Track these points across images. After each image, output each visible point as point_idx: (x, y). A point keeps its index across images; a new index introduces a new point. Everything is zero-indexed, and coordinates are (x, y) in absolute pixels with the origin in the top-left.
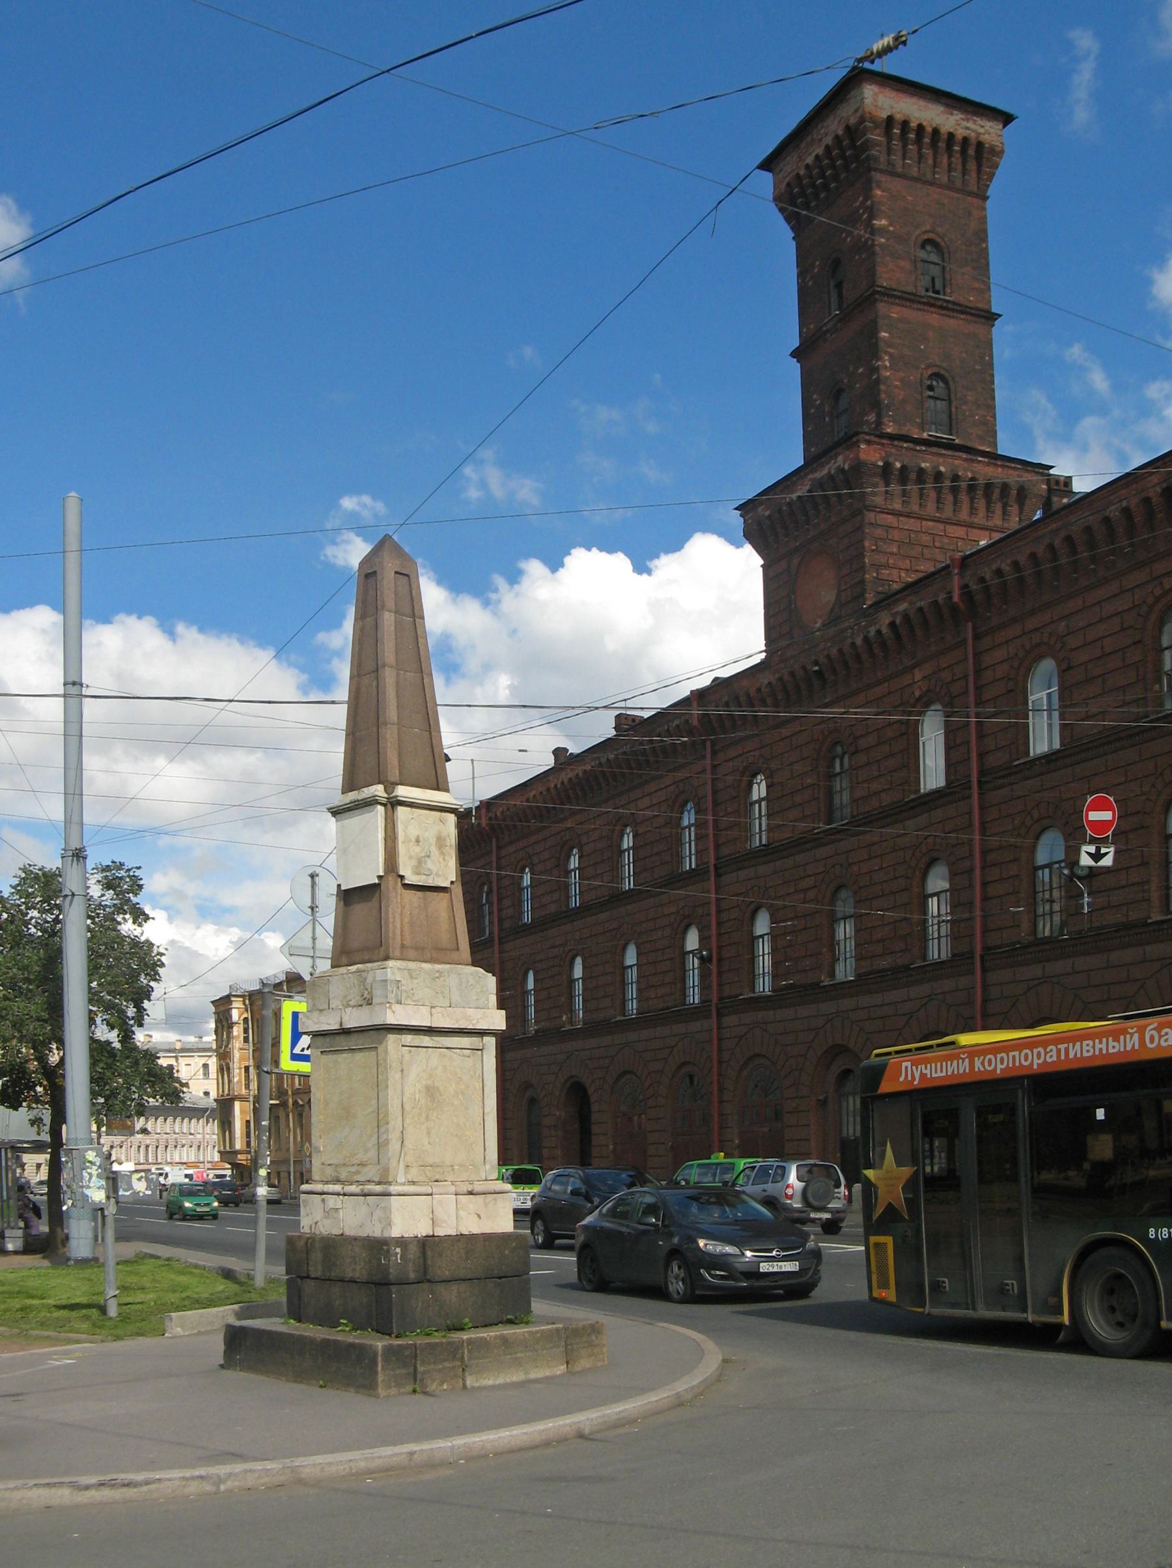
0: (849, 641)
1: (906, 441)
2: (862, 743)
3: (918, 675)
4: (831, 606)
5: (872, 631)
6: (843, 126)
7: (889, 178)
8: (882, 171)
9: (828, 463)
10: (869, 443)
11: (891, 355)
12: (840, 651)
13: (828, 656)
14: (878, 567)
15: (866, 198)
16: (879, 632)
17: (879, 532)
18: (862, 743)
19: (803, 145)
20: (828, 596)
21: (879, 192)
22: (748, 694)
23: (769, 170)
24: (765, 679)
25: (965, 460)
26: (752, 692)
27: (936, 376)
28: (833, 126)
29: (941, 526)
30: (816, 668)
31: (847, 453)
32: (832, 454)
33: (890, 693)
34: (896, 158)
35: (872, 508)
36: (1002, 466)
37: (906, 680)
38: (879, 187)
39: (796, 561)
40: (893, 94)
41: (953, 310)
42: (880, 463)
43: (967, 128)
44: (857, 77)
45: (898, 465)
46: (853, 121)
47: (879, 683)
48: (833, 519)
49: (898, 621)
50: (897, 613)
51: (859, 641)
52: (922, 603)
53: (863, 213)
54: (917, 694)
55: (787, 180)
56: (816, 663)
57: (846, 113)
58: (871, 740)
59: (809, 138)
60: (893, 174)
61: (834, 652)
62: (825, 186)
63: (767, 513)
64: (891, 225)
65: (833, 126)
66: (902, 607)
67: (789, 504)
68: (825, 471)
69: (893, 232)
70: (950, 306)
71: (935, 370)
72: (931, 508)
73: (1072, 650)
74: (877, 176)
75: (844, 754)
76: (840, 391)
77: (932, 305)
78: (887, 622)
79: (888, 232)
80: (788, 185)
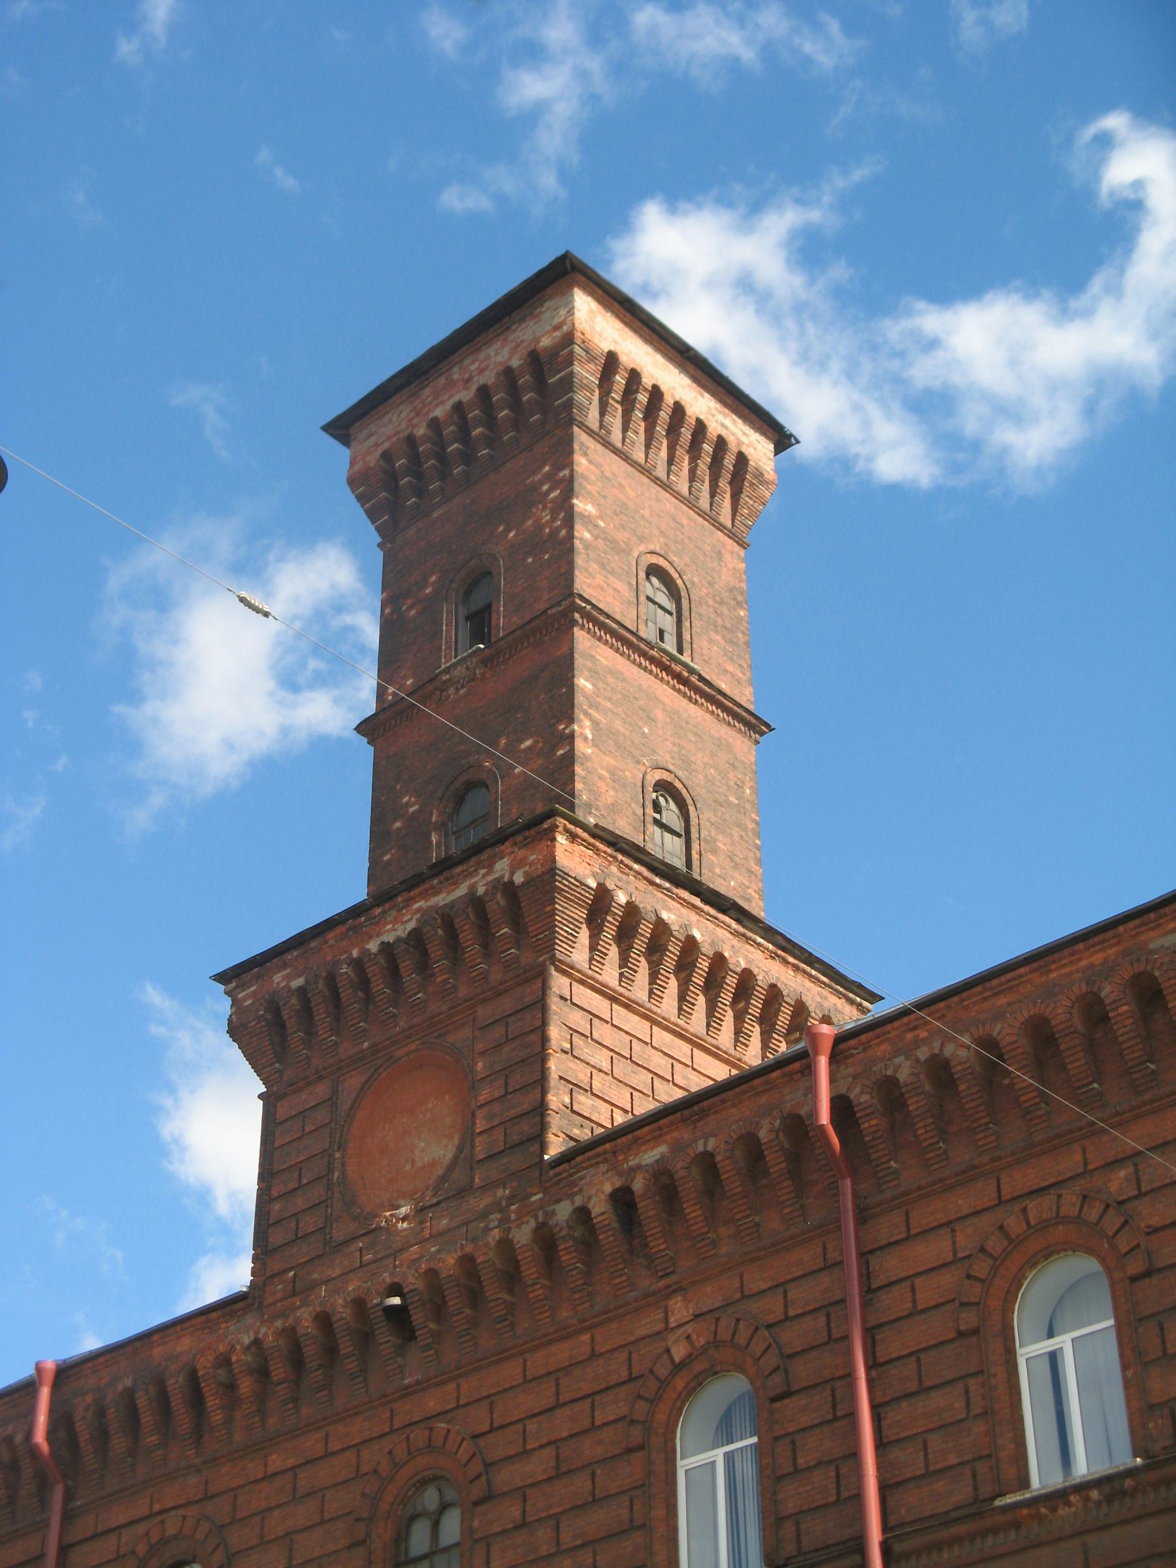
0: (496, 1234)
1: (638, 861)
2: (506, 1477)
3: (680, 1310)
4: (440, 1171)
5: (564, 1211)
6: (523, 352)
7: (599, 447)
8: (590, 432)
9: (470, 875)
10: (573, 837)
11: (596, 724)
12: (467, 1261)
13: (432, 1273)
14: (574, 1087)
15: (558, 468)
16: (583, 1214)
17: (578, 1020)
18: (506, 1477)
19: (427, 391)
20: (434, 1150)
21: (584, 461)
22: (193, 1379)
23: (345, 440)
24: (242, 1333)
25: (735, 934)
26: (204, 1365)
27: (663, 787)
28: (502, 354)
29: (686, 1048)
30: (396, 1301)
31: (520, 853)
32: (484, 856)
33: (594, 1356)
34: (615, 422)
35: (567, 970)
36: (796, 968)
37: (648, 1323)
38: (585, 454)
39: (352, 1083)
40: (618, 325)
41: (697, 690)
42: (594, 885)
43: (723, 425)
44: (564, 273)
45: (622, 898)
46: (545, 342)
47: (566, 1334)
48: (463, 991)
49: (638, 1185)
50: (639, 1167)
51: (523, 1235)
52: (711, 1144)
53: (551, 490)
54: (679, 1352)
55: (386, 446)
56: (395, 1290)
57: (536, 332)
58: (537, 1466)
59: (442, 380)
60: (607, 444)
61: (449, 1262)
62: (467, 457)
63: (298, 982)
64: (601, 517)
65: (502, 354)
66: (651, 1156)
67: (358, 965)
68: (462, 890)
69: (604, 531)
70: (694, 679)
71: (668, 777)
72: (668, 1006)
73: (1153, 1231)
74: (580, 436)
75: (444, 1507)
76: (471, 786)
77: (666, 669)
78: (608, 1188)
79: (596, 526)
80: (386, 456)
